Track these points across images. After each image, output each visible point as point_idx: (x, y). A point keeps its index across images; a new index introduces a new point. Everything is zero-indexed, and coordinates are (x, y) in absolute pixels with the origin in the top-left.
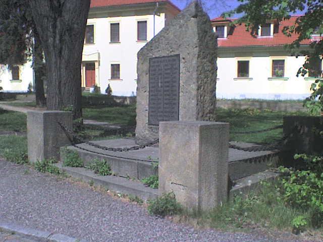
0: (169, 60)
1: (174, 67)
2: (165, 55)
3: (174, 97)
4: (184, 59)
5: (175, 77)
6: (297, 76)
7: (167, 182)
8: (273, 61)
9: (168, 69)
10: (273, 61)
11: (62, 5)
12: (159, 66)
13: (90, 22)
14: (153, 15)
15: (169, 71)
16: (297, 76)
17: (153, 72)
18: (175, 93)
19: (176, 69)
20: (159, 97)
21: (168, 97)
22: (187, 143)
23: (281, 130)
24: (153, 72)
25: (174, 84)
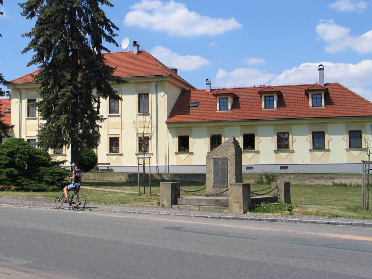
0: (223, 160)
1: (225, 162)
2: (221, 157)
3: (225, 175)
4: (229, 159)
5: (225, 167)
6: (262, 170)
7: (232, 202)
8: (246, 167)
9: (222, 163)
10: (246, 167)
11: (221, 211)
12: (218, 162)
13: (108, 98)
14: (170, 173)
15: (222, 164)
16: (262, 170)
17: (215, 164)
18: (226, 173)
19: (226, 163)
20: (218, 175)
21: (222, 175)
22: (238, 190)
23: (168, 173)
24: (215, 164)
25: (225, 169)
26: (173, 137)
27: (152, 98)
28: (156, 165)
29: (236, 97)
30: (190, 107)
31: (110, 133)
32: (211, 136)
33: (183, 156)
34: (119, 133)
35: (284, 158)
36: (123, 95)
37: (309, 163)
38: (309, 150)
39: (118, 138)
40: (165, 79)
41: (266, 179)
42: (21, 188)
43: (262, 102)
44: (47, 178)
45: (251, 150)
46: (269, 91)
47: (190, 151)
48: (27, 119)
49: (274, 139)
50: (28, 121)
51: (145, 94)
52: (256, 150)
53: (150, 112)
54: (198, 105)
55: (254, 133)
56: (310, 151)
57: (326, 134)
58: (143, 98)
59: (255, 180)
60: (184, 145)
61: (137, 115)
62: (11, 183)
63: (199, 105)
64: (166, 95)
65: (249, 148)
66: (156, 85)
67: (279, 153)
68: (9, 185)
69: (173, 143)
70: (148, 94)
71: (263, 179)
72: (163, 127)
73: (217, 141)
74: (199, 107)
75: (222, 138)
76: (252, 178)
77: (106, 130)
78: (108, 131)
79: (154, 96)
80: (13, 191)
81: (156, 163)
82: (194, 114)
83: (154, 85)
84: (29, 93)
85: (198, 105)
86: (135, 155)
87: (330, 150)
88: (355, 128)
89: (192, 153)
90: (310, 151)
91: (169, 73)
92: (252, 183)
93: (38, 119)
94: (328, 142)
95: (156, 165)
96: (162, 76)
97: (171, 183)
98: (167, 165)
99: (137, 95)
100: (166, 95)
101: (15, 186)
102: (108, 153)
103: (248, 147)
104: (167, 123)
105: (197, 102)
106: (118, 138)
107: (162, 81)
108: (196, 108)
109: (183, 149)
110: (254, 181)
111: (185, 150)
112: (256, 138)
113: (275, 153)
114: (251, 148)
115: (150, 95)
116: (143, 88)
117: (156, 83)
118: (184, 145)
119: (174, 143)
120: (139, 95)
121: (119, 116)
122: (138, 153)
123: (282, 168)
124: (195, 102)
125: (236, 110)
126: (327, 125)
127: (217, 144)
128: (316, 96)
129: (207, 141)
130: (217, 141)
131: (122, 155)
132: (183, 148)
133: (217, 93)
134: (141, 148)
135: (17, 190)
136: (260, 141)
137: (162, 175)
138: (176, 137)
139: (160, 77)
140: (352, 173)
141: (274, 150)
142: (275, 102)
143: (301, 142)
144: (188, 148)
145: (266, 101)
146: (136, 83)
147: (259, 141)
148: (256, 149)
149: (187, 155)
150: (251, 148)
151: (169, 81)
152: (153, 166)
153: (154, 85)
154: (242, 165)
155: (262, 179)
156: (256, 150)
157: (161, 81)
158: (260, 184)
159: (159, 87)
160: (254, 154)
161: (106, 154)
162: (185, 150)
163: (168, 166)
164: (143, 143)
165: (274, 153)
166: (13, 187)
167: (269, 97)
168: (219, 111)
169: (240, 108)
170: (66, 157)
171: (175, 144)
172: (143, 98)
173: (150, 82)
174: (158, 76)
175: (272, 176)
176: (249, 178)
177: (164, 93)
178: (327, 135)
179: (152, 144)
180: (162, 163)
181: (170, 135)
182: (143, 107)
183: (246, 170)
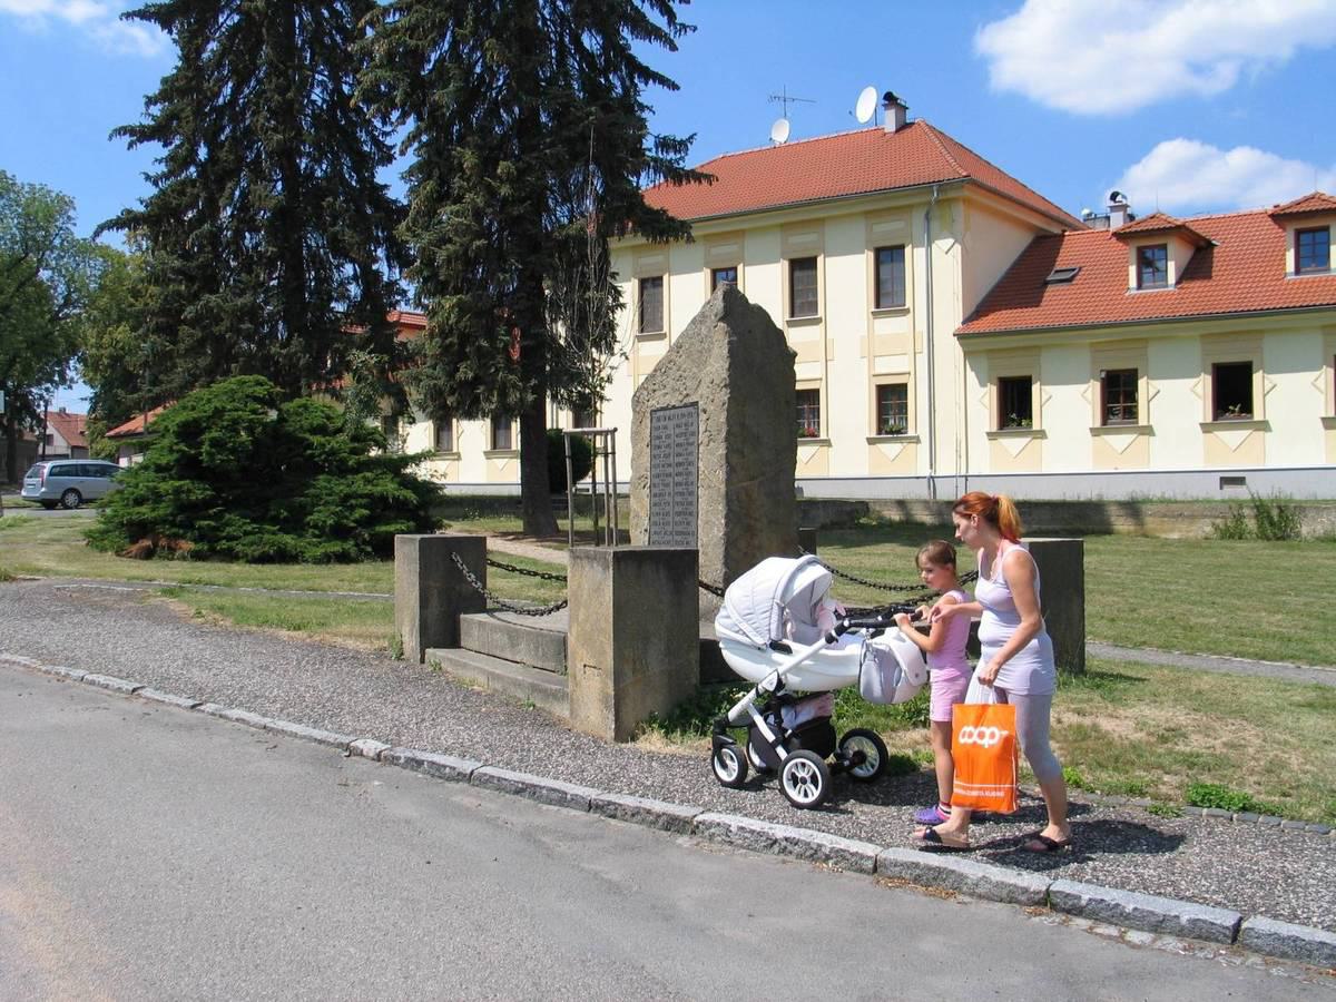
8: (1221, 478)
26: (983, 384)
27: (915, 257)
28: (927, 474)
29: (1202, 243)
30: (1046, 283)
31: (878, 371)
32: (1103, 375)
33: (1013, 444)
34: (906, 370)
35: (1233, 448)
36: (917, 247)
37: (866, 475)
38: (1201, 424)
39: (904, 386)
40: (951, 195)
41: (1253, 521)
42: (214, 549)
43: (1284, 255)
44: (322, 516)
45: (1239, 417)
46: (1310, 211)
47: (1036, 426)
48: (640, 339)
49: (1323, 376)
50: (876, 321)
51: (726, 270)
52: (1140, 424)
53: (909, 304)
54: (1073, 277)
55: (1247, 360)
56: (1206, 428)
57: (1142, 377)
58: (888, 257)
59: (1213, 524)
60: (1015, 406)
61: (871, 315)
62: (181, 531)
63: (1078, 277)
64: (958, 248)
65: (1233, 412)
66: (927, 218)
67: (1105, 437)
68: (176, 536)
69: (1313, 384)
70: (902, 247)
71: (1246, 520)
72: (950, 352)
73: (1125, 391)
74: (1074, 282)
75: (1140, 382)
76: (1206, 516)
77: (865, 360)
78: (871, 365)
79: (920, 252)
80: (184, 558)
81: (929, 466)
82: (1057, 304)
83: (918, 218)
84: (714, 251)
85: (1073, 277)
86: (1320, 424)
87: (1047, 432)
88: (1015, 371)
89: (1042, 434)
90: (1206, 428)
91: (964, 174)
92: (1204, 535)
93: (911, 314)
94: (1149, 402)
95: (926, 472)
96: (943, 186)
97: (419, 537)
98: (963, 473)
99: (871, 255)
100: (960, 247)
101: (195, 541)
102: (874, 435)
103: (1231, 408)
104: (961, 337)
105: (1073, 267)
106: (904, 386)
107: (944, 201)
108: (1064, 286)
109: (1013, 420)
110: (1209, 529)
111: (1020, 424)
112: (1257, 377)
113: (869, 444)
114: (1241, 411)
115: (908, 250)
116: (887, 231)
117: (926, 209)
118: (1015, 406)
119: (985, 400)
120: (714, 272)
121: (818, 321)
122: (874, 435)
123: (1225, 481)
124: (1069, 267)
125: (1196, 286)
126: (1146, 347)
127: (1124, 402)
128: (1311, 235)
129: (1089, 395)
130: (1125, 391)
131: (827, 443)
132: (1014, 416)
133: (1290, 210)
134: (887, 421)
135: (197, 556)
136: (1048, 397)
137: (909, 506)
138: (1205, 373)
139: (935, 188)
140: (1329, 498)
141: (1324, 416)
142: (1169, 263)
143: (1176, 400)
144: (1029, 417)
145: (1301, 248)
146: (867, 214)
147: (1045, 397)
148: (1142, 421)
149: (1246, 433)
150: (1241, 411)
151: (968, 202)
152: (918, 478)
153: (918, 218)
154: (795, 480)
155: (1239, 518)
156: (1140, 424)
157: (938, 202)
158: (1232, 536)
159: (935, 225)
160: (1250, 431)
161: (868, 439)
162: (1020, 424)
163: (966, 477)
164: (891, 401)
165: (1323, 430)
166: (187, 546)
167: (1313, 230)
168: (1136, 292)
169: (1210, 277)
170: (1268, 435)
171: (1323, 387)
172: (888, 257)
173: (911, 207)
174: (926, 187)
175: (1279, 507)
176: (1193, 517)
177: (951, 241)
178: (1261, 372)
179: (917, 402)
180: (945, 467)
181: (971, 375)
182: (887, 294)
183: (1221, 488)
